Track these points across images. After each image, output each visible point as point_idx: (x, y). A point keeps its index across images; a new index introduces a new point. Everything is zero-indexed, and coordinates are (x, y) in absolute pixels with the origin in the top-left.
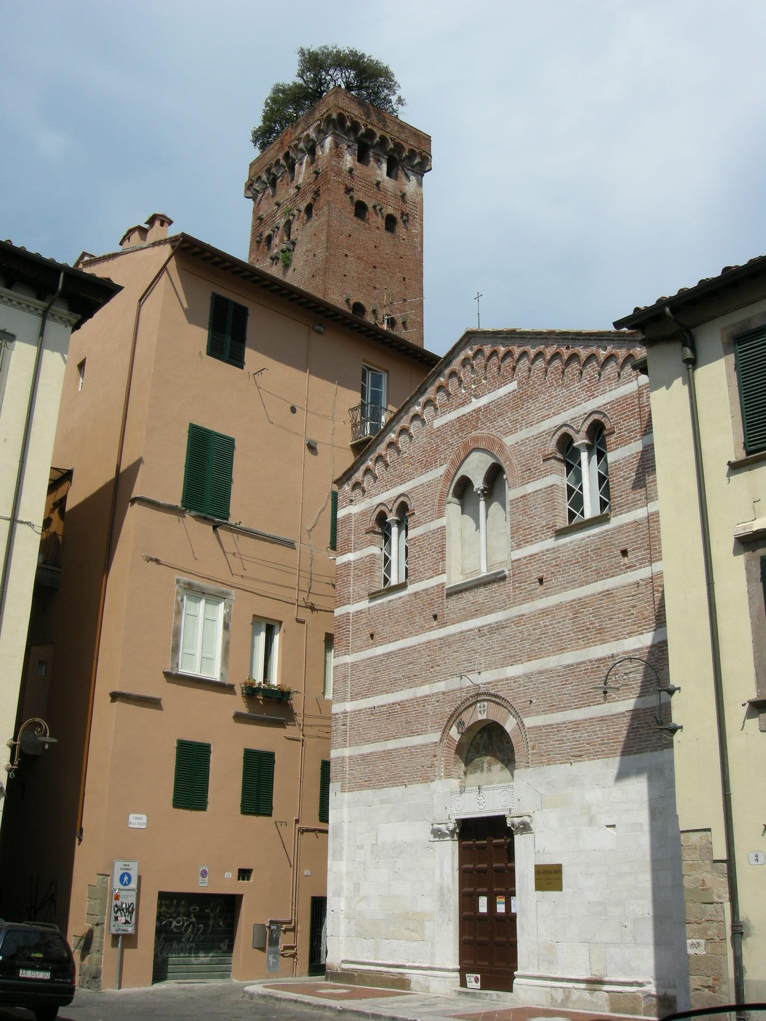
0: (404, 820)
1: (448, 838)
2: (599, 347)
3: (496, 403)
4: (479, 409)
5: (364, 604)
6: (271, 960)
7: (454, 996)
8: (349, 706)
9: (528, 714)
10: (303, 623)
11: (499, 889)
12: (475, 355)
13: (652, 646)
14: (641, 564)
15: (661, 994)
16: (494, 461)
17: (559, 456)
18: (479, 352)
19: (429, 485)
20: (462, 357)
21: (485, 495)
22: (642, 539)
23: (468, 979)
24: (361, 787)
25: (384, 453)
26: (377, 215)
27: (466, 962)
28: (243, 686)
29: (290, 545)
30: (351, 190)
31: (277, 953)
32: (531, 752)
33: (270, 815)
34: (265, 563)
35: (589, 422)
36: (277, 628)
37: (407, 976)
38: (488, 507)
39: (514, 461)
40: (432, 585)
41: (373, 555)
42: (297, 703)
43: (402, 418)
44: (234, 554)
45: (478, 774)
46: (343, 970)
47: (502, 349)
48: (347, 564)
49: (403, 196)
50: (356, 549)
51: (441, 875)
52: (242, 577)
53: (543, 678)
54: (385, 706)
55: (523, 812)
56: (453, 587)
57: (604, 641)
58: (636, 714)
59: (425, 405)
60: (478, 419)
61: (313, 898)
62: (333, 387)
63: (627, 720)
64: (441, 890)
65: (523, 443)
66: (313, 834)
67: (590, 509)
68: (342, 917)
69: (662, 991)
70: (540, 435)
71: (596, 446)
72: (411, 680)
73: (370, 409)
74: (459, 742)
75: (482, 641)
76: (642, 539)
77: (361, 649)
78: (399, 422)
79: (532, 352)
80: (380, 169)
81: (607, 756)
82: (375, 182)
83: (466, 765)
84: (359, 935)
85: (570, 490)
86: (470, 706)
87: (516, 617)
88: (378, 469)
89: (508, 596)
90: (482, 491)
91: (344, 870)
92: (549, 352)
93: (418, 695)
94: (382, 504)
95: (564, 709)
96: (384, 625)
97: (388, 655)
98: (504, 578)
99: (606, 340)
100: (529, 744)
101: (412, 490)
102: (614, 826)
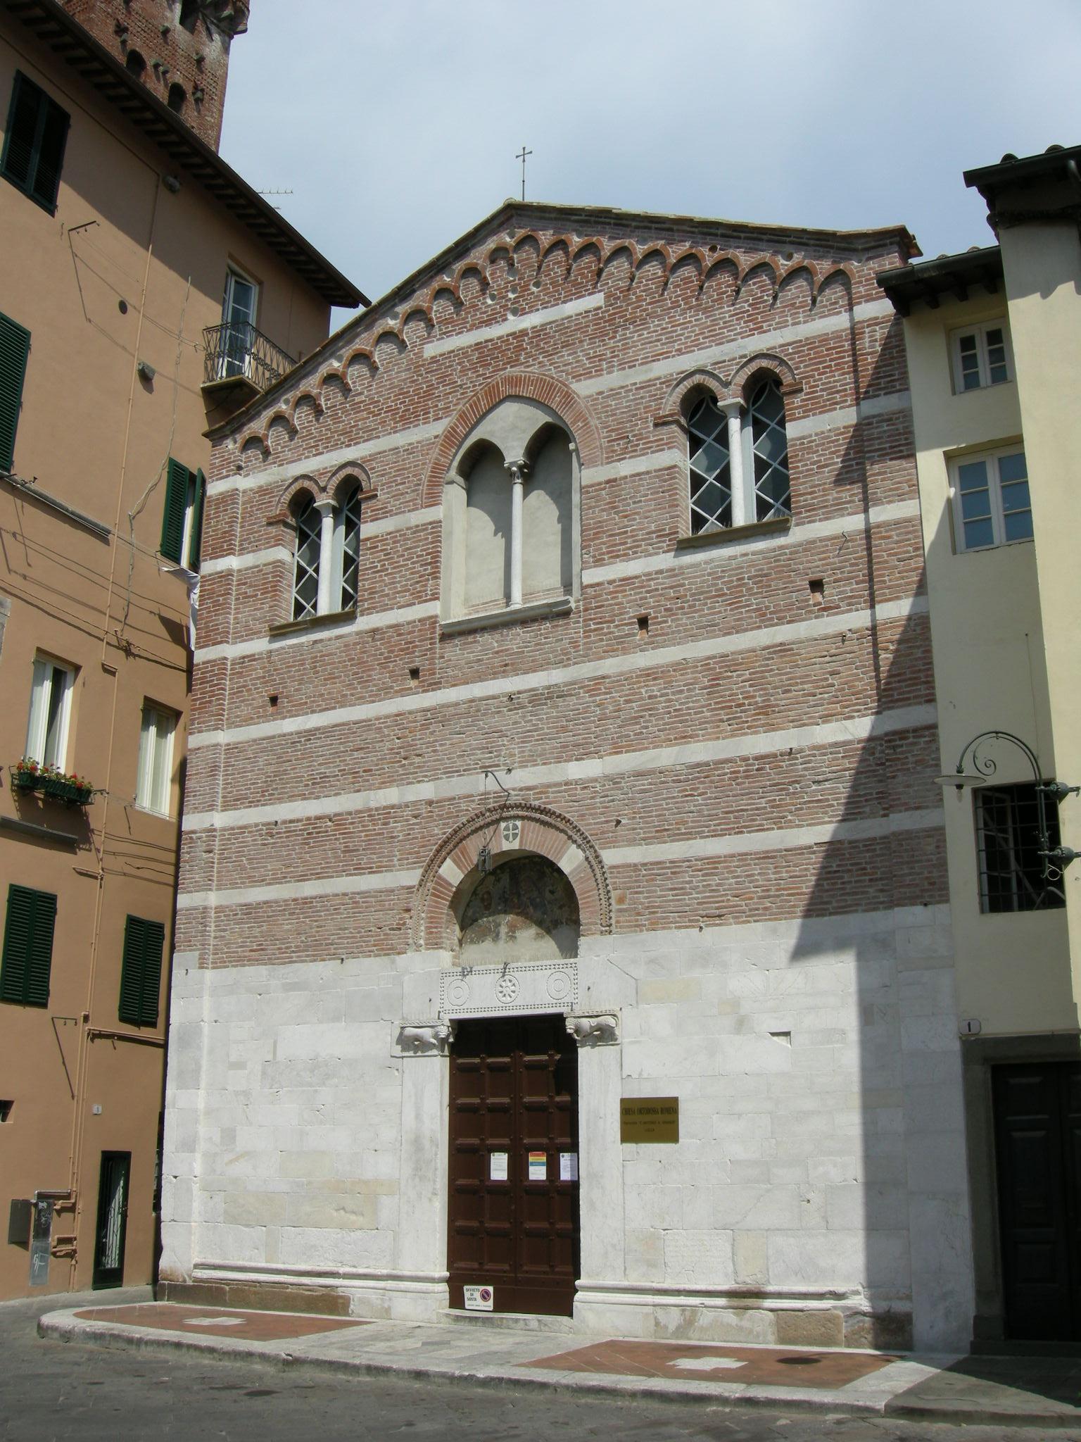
0: (336, 1019)
1: (435, 1052)
2: (776, 253)
3: (561, 326)
4: (524, 333)
5: (260, 645)
6: (37, 1263)
7: (446, 1324)
8: (220, 819)
9: (613, 843)
10: (113, 674)
11: (533, 1140)
12: (520, 244)
13: (870, 739)
14: (849, 604)
15: (881, 1311)
16: (549, 419)
17: (683, 421)
18: (529, 240)
19: (410, 450)
20: (491, 244)
21: (523, 475)
22: (852, 565)
23: (467, 1295)
24: (241, 961)
25: (315, 392)
26: (158, 80)
27: (461, 1264)
28: (15, 771)
29: (101, 535)
30: (125, 30)
31: (45, 1250)
32: (615, 907)
33: (44, 1005)
34: (62, 561)
35: (749, 370)
36: (70, 677)
37: (340, 1292)
38: (526, 494)
39: (594, 422)
40: (410, 618)
41: (278, 564)
42: (98, 813)
43: (358, 335)
44: (14, 535)
45: (487, 944)
46: (197, 1280)
47: (576, 241)
48: (226, 575)
49: (200, 60)
50: (243, 551)
51: (418, 1117)
52: (25, 577)
53: (644, 783)
54: (298, 821)
55: (597, 1009)
56: (459, 623)
57: (771, 728)
58: (833, 849)
59: (409, 318)
60: (520, 348)
61: (103, 1152)
62: (186, 286)
63: (816, 859)
64: (417, 1143)
65: (614, 393)
66: (109, 1042)
67: (328, 601)
68: (196, 1188)
69: (883, 1306)
70: (648, 384)
71: (752, 412)
72: (358, 779)
74: (458, 888)
75: (516, 716)
76: (852, 565)
77: (248, 721)
78: (350, 341)
79: (640, 250)
80: (172, 10)
81: (776, 917)
82: (161, 29)
83: (462, 929)
84: (232, 1219)
85: (301, 572)
86: (488, 825)
87: (590, 679)
88: (301, 418)
89: (574, 643)
90: (521, 468)
91: (201, 1106)
92: (675, 252)
93: (373, 804)
94: (305, 477)
95: (688, 836)
96: (301, 682)
97: (310, 734)
98: (566, 614)
99: (792, 243)
100: (613, 894)
101: (373, 457)
102: (787, 1034)
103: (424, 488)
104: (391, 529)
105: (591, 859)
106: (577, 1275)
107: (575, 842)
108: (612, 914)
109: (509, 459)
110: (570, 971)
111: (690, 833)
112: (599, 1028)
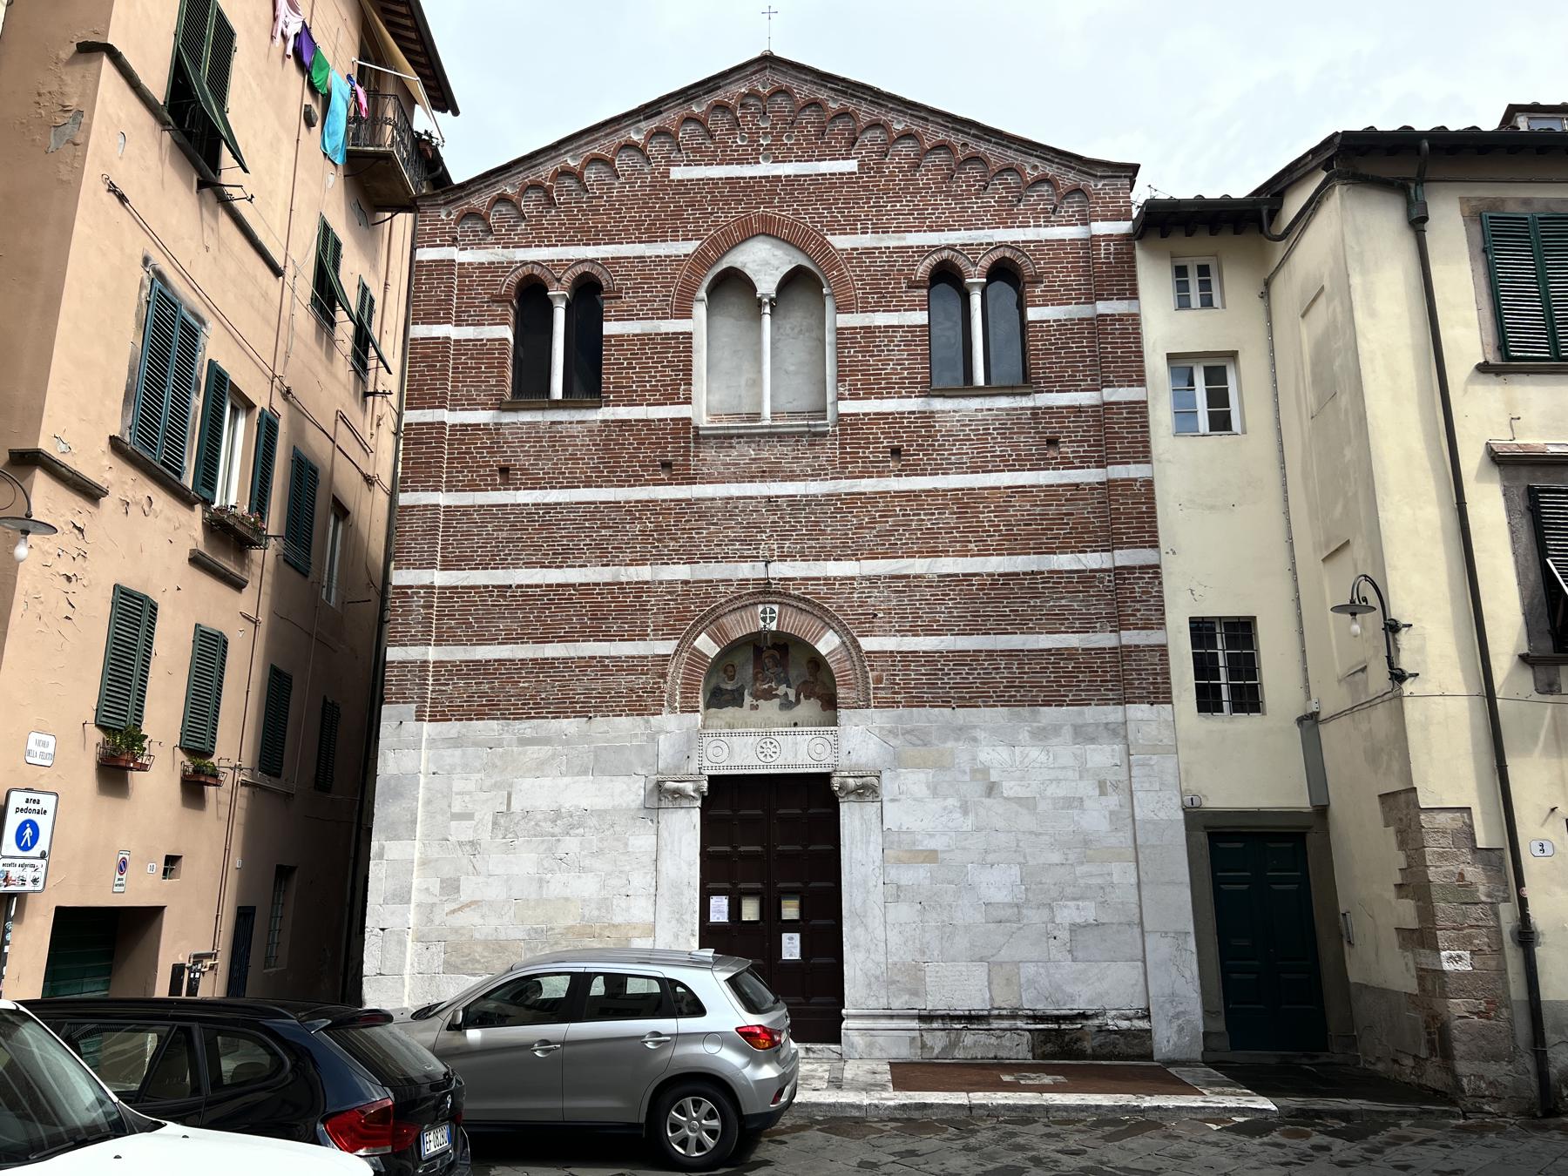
0: (585, 773)
53: (901, 584)
60: (773, 193)
73: (1410, 204)
88: (529, 205)
96: (538, 458)
103: (673, 300)
104: (638, 331)
109: (760, 291)
110: (831, 738)
112: (863, 787)
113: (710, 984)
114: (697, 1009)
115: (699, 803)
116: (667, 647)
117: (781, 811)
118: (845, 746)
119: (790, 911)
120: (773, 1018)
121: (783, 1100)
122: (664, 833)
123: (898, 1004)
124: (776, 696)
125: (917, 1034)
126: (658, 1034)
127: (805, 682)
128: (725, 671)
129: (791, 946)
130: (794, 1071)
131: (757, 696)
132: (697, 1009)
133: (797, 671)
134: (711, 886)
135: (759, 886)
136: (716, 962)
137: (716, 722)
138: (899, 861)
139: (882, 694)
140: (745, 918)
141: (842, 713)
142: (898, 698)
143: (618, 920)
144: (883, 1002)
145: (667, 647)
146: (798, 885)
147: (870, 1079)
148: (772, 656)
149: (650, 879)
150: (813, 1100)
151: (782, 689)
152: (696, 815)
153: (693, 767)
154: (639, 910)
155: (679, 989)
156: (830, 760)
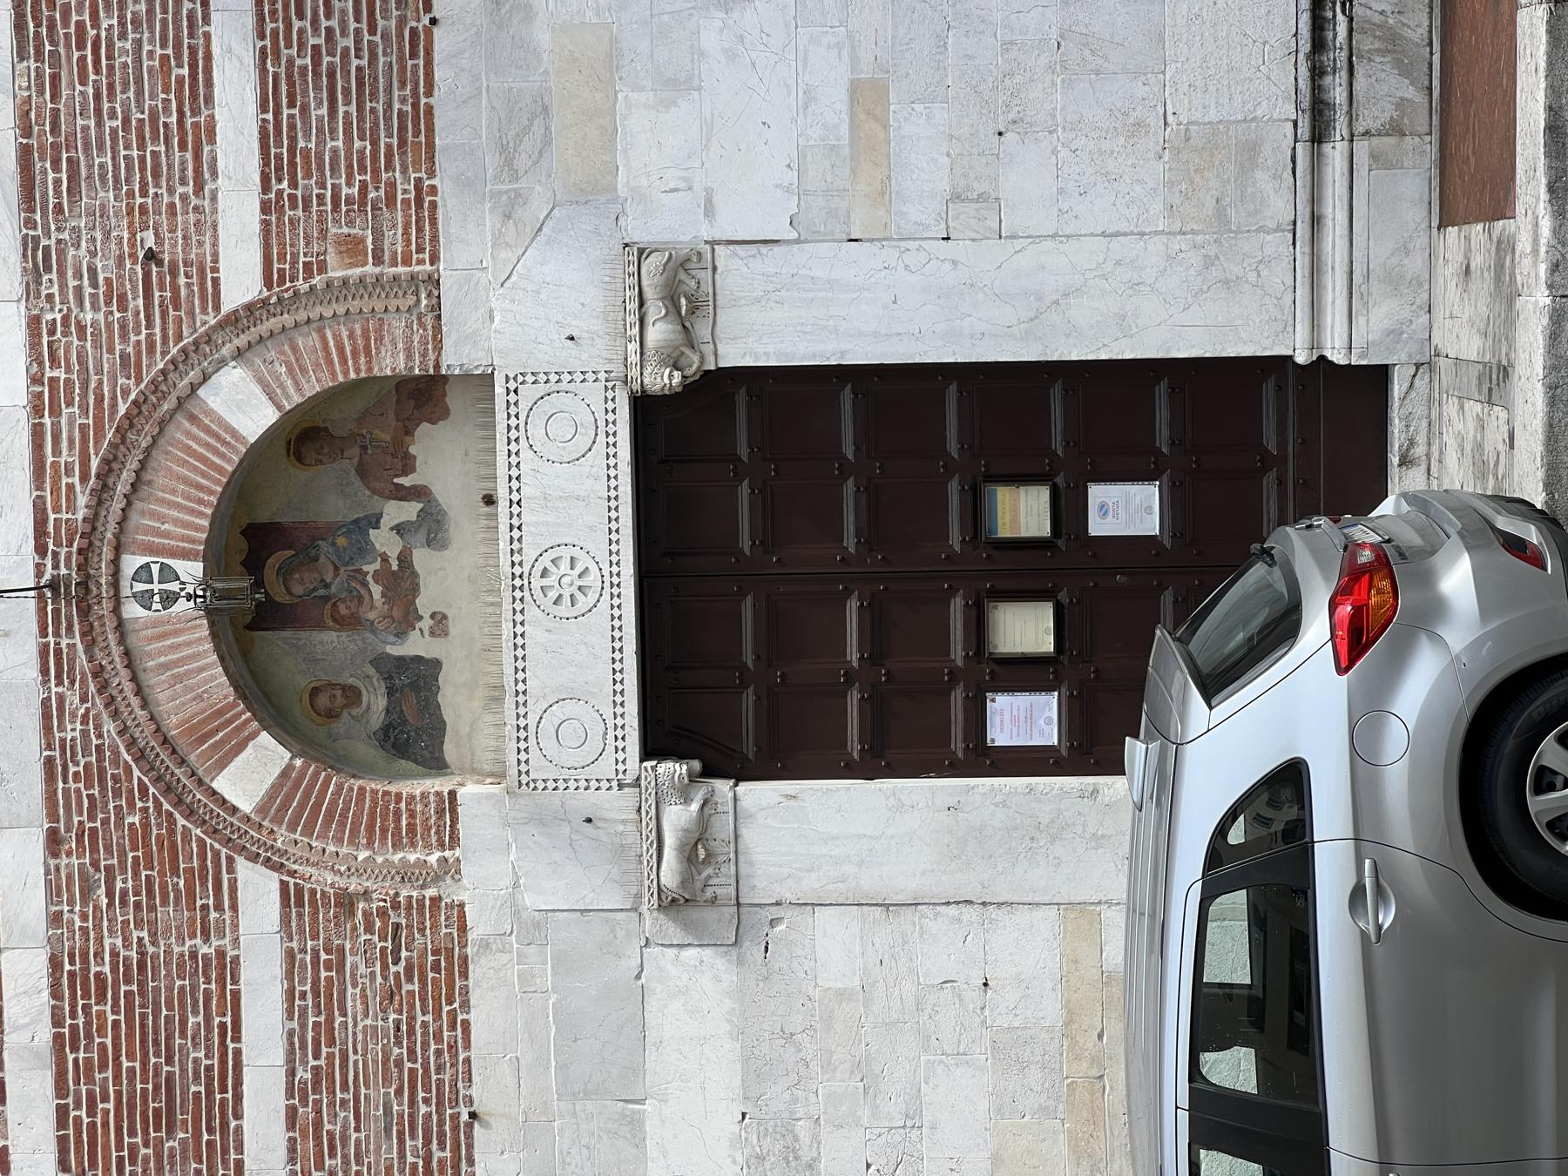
0: (636, 1124)
53: (49, 177)
105: (241, 341)
106: (1282, 363)
107: (194, 388)
108: (328, 313)
110: (528, 393)
111: (193, 50)
112: (671, 297)
113: (1220, 747)
114: (1289, 781)
115: (723, 786)
116: (258, 890)
117: (745, 544)
118: (550, 353)
119: (1024, 512)
120: (1310, 558)
121: (1532, 534)
122: (809, 886)
123: (1279, 201)
124: (405, 559)
125: (1361, 147)
126: (1357, 894)
127: (362, 472)
128: (331, 715)
129: (1127, 509)
130: (1459, 505)
131: (405, 618)
132: (1289, 781)
133: (327, 494)
134: (958, 745)
135: (957, 604)
136: (1160, 731)
137: (484, 740)
138: (883, 194)
139: (394, 240)
140: (1047, 645)
141: (455, 358)
142: (405, 189)
143: (1052, 1012)
144: (1277, 244)
145: (258, 890)
146: (954, 487)
147: (1482, 285)
148: (285, 572)
149: (939, 923)
150: (1539, 448)
151: (384, 541)
152: (756, 793)
153: (617, 806)
154: (1027, 951)
155: (1236, 836)
156: (594, 394)
